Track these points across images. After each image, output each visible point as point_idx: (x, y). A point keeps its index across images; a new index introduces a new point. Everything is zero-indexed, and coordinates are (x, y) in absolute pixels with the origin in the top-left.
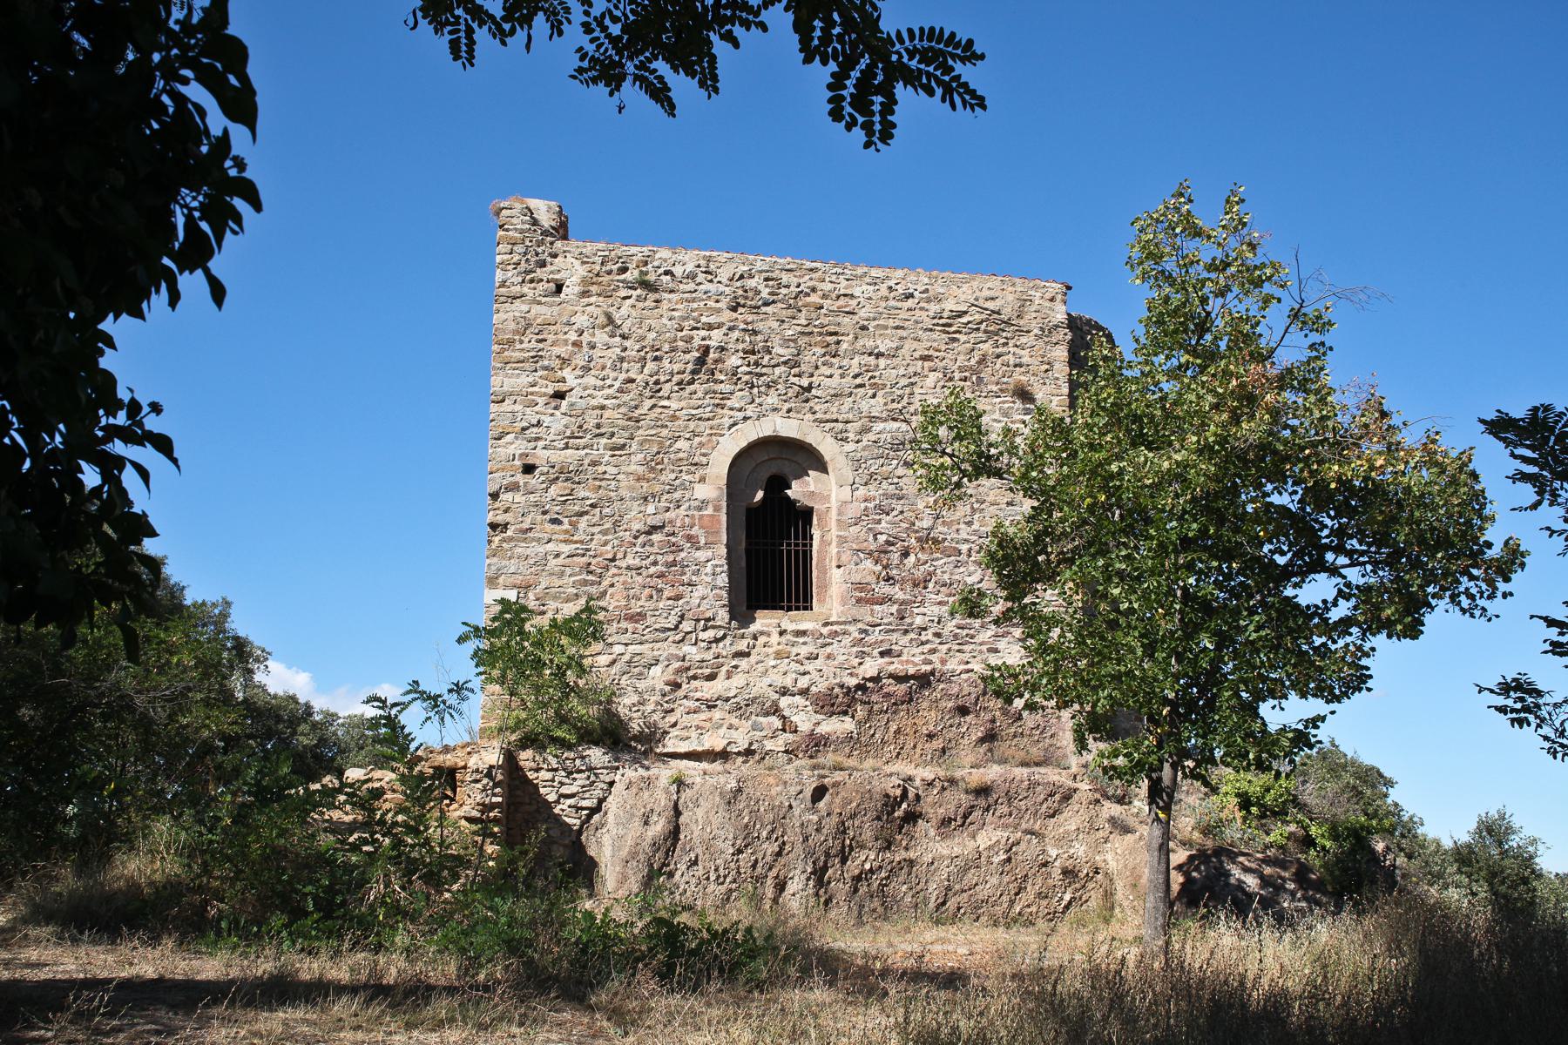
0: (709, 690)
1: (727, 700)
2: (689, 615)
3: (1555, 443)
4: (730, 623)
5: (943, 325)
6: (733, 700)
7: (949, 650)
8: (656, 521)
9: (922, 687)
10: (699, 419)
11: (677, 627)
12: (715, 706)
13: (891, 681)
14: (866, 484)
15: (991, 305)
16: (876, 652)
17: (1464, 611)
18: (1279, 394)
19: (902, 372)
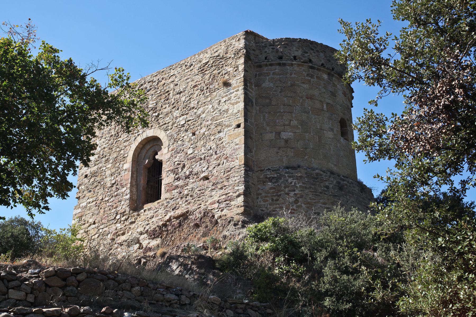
0: (123, 238)
1: (126, 241)
2: (119, 212)
3: (5, 118)
4: (129, 212)
5: (201, 71)
6: (128, 241)
7: (195, 201)
8: (113, 182)
9: (185, 219)
10: (127, 141)
11: (115, 218)
12: (123, 245)
13: (175, 220)
14: (173, 144)
15: (217, 54)
16: (171, 210)
17: (385, 48)
18: (78, 167)
19: (187, 95)
